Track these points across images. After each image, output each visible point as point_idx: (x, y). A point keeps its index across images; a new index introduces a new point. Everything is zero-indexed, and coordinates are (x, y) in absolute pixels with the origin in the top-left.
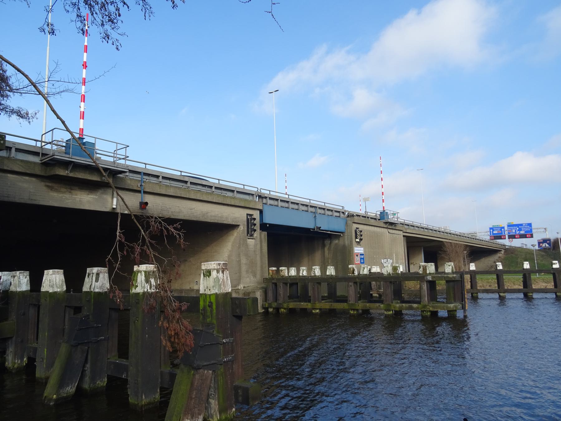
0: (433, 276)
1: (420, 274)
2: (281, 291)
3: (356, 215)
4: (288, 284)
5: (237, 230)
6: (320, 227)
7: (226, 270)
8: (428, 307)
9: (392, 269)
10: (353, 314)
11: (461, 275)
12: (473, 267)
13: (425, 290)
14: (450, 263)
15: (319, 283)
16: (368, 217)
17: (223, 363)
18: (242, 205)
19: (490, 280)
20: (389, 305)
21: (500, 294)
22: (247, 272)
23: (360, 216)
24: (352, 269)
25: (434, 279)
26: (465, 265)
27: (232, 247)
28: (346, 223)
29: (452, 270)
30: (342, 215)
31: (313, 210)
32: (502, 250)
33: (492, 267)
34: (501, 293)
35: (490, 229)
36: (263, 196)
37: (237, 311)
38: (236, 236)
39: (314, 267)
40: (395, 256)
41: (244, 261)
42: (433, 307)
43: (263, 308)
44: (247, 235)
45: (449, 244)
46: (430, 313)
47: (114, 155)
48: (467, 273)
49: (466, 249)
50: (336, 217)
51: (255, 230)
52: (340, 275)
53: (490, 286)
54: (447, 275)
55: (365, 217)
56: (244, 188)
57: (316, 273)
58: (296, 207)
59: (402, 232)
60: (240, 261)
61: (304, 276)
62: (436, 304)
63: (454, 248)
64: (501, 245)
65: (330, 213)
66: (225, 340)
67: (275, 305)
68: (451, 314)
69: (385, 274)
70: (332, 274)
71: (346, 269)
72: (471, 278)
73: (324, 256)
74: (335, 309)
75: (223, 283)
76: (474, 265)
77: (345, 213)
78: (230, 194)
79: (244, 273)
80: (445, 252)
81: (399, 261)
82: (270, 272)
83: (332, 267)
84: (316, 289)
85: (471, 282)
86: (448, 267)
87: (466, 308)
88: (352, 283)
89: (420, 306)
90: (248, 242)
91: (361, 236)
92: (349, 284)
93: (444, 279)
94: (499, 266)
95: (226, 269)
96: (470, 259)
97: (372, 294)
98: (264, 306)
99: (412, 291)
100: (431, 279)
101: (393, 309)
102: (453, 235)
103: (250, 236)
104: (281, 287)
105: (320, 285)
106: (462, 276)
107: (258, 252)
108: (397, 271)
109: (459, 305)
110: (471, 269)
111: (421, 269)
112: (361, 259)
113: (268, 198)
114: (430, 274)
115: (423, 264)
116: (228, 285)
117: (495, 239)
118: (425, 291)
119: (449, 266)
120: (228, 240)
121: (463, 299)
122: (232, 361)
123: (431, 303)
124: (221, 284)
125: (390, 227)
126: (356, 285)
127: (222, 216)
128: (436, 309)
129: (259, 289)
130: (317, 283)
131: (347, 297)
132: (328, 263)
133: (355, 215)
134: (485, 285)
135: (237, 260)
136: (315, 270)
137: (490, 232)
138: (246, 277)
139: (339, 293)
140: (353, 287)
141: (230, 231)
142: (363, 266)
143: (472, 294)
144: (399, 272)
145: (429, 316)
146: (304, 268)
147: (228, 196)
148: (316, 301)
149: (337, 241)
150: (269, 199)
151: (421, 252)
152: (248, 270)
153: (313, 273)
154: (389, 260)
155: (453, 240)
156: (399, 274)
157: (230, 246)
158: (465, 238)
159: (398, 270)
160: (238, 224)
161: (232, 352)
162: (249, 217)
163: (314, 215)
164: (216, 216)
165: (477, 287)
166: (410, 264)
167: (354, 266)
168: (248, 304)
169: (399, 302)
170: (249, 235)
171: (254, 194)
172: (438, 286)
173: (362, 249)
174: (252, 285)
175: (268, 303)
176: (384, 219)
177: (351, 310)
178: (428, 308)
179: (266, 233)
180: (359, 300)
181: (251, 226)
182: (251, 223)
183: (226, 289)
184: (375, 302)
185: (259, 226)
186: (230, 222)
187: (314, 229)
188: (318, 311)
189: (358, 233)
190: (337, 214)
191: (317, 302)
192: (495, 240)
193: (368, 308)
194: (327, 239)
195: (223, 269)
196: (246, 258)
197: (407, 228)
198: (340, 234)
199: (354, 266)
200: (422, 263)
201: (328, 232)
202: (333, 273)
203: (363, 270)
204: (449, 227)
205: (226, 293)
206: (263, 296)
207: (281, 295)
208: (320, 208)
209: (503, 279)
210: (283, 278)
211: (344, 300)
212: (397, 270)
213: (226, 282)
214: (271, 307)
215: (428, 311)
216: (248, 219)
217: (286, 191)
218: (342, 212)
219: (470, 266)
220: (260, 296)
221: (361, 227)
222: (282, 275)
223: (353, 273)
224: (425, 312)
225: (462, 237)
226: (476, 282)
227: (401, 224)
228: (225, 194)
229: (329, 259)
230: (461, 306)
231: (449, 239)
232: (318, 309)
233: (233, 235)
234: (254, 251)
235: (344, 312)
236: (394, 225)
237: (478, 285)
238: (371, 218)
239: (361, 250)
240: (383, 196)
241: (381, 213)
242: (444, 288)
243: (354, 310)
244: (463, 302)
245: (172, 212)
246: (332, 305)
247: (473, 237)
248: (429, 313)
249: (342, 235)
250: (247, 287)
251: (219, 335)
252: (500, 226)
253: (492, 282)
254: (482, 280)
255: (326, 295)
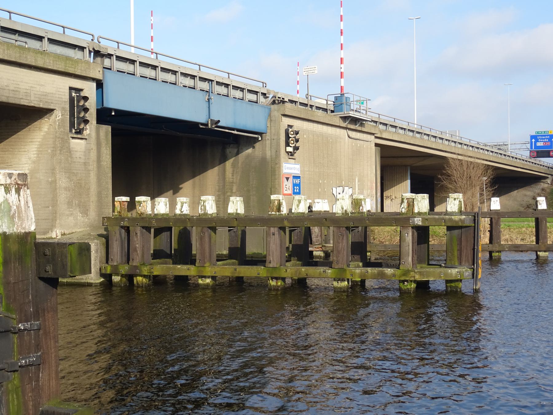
0: (424, 218)
1: (404, 214)
2: (137, 242)
3: (289, 100)
4: (152, 230)
5: (49, 119)
6: (219, 121)
7: (26, 188)
8: (412, 273)
9: (352, 203)
10: (276, 286)
11: (475, 217)
12: (496, 204)
13: (409, 244)
14: (455, 195)
15: (214, 229)
16: (311, 106)
17: (17, 368)
18: (61, 68)
19: (524, 229)
20: (343, 270)
21: (538, 253)
22: (70, 204)
23: (296, 102)
24: (276, 202)
25: (427, 224)
26: (482, 202)
27: (38, 154)
28: (270, 115)
29: (460, 208)
30: (262, 99)
31: (205, 86)
32: (549, 176)
33: (529, 208)
34: (540, 251)
35: (532, 137)
36: (103, 51)
37: (48, 268)
38: (46, 132)
39: (203, 198)
40: (358, 182)
41: (63, 182)
42: (421, 273)
43: (102, 275)
44: (71, 131)
45: (457, 162)
46: (415, 285)
48: (485, 215)
49: (487, 172)
50: (250, 102)
51: (86, 122)
52: (255, 213)
53: (522, 239)
54: (450, 217)
55: (306, 105)
56: (64, 32)
57: (207, 208)
58: (170, 78)
59: (373, 137)
60: (55, 182)
61: (185, 215)
62: (427, 268)
63: (465, 169)
64: (547, 168)
65: (238, 94)
66: (24, 325)
67: (124, 269)
68: (451, 287)
69: (338, 214)
70: (239, 212)
71: (265, 201)
72: (491, 225)
73: (224, 178)
74: (242, 277)
75: (19, 213)
76: (499, 201)
77: (267, 95)
78: (33, 44)
79: (62, 207)
80: (450, 176)
81: (365, 192)
82: (117, 204)
83: (238, 198)
84: (207, 239)
85: (491, 231)
86: (453, 201)
87: (479, 276)
88: (276, 229)
89: (398, 272)
90: (72, 146)
91: (297, 141)
92: (270, 230)
93: (443, 224)
94: (540, 204)
95: (25, 185)
96: (493, 190)
97: (312, 252)
98: (103, 272)
99: (385, 246)
100: (420, 223)
101: (350, 277)
102: (465, 147)
103: (76, 133)
104: (139, 234)
105: (215, 233)
106: (476, 218)
107: (93, 166)
108: (361, 208)
109: (466, 271)
110: (493, 208)
111: (405, 205)
112: (294, 185)
113: (114, 57)
114: (419, 214)
115: (409, 195)
116: (30, 218)
117: (538, 157)
118: (409, 246)
119: (455, 199)
120: (30, 140)
121: (474, 261)
122: (37, 365)
123: (418, 268)
124: (14, 214)
125: (352, 127)
126: (283, 233)
127: (16, 89)
128: (427, 278)
129: (94, 239)
130: (209, 228)
131: (265, 257)
132: (232, 192)
133: (286, 100)
134: (515, 238)
135: (48, 181)
136: (206, 204)
137: (531, 142)
138: (67, 215)
139: (251, 249)
140: (277, 236)
141: (35, 121)
142: (297, 197)
143: (491, 253)
144: (365, 210)
145: (412, 290)
146: (184, 199)
147: (29, 49)
148: (205, 263)
149: (250, 151)
150: (116, 59)
151: (406, 176)
152: (72, 201)
153: (201, 209)
154: (346, 188)
155: (465, 156)
156: (363, 213)
157: (35, 152)
158: (486, 152)
159: (363, 207)
160: (52, 107)
161: (38, 347)
162: (74, 94)
163: (207, 97)
164: (4, 89)
165: (500, 241)
166: (384, 198)
167: (280, 197)
168: (71, 255)
169: (361, 264)
170: (74, 131)
171: (86, 48)
172: (432, 237)
173: (298, 166)
174: (78, 230)
175: (112, 266)
176: (342, 111)
177: (272, 278)
178: (412, 275)
179: (109, 128)
180: (287, 261)
181: (79, 113)
182: (78, 106)
183: (24, 226)
184: (316, 264)
185: (95, 113)
186: (33, 101)
187: (206, 125)
188: (208, 281)
189: (290, 136)
190: (253, 97)
191: (207, 264)
192: (538, 159)
193: (303, 275)
194: (232, 145)
195: (18, 184)
196: (68, 178)
197: (383, 131)
198: (256, 136)
199: (280, 197)
200: (406, 193)
201: (233, 132)
202: (241, 210)
203: (298, 206)
204: (459, 131)
205: (26, 233)
206: (101, 253)
207: (137, 251)
208: (218, 83)
209: (546, 227)
210: (143, 218)
211: (259, 260)
212: (361, 205)
213: (25, 211)
214: (117, 274)
215: (411, 281)
216: (72, 99)
217: (152, 45)
218: (262, 93)
219: (492, 203)
220: (95, 252)
221: (297, 124)
222: (139, 212)
223: (279, 210)
224: (406, 283)
225: (481, 151)
226: (500, 232)
227: (373, 121)
228: (24, 44)
229: (234, 184)
230: (470, 271)
231: (458, 154)
232: (209, 277)
233: (40, 129)
234: (85, 164)
235: (262, 284)
236: (360, 123)
237: (503, 238)
238: (316, 107)
239: (294, 168)
240: (342, 66)
241: (336, 98)
242: (443, 243)
243: (277, 278)
244: (474, 265)
246: (235, 270)
247: (500, 148)
248: (413, 285)
249: (260, 139)
250: (69, 234)
251: (10, 315)
252: (550, 133)
253: (528, 232)
254: (510, 229)
255: (225, 252)
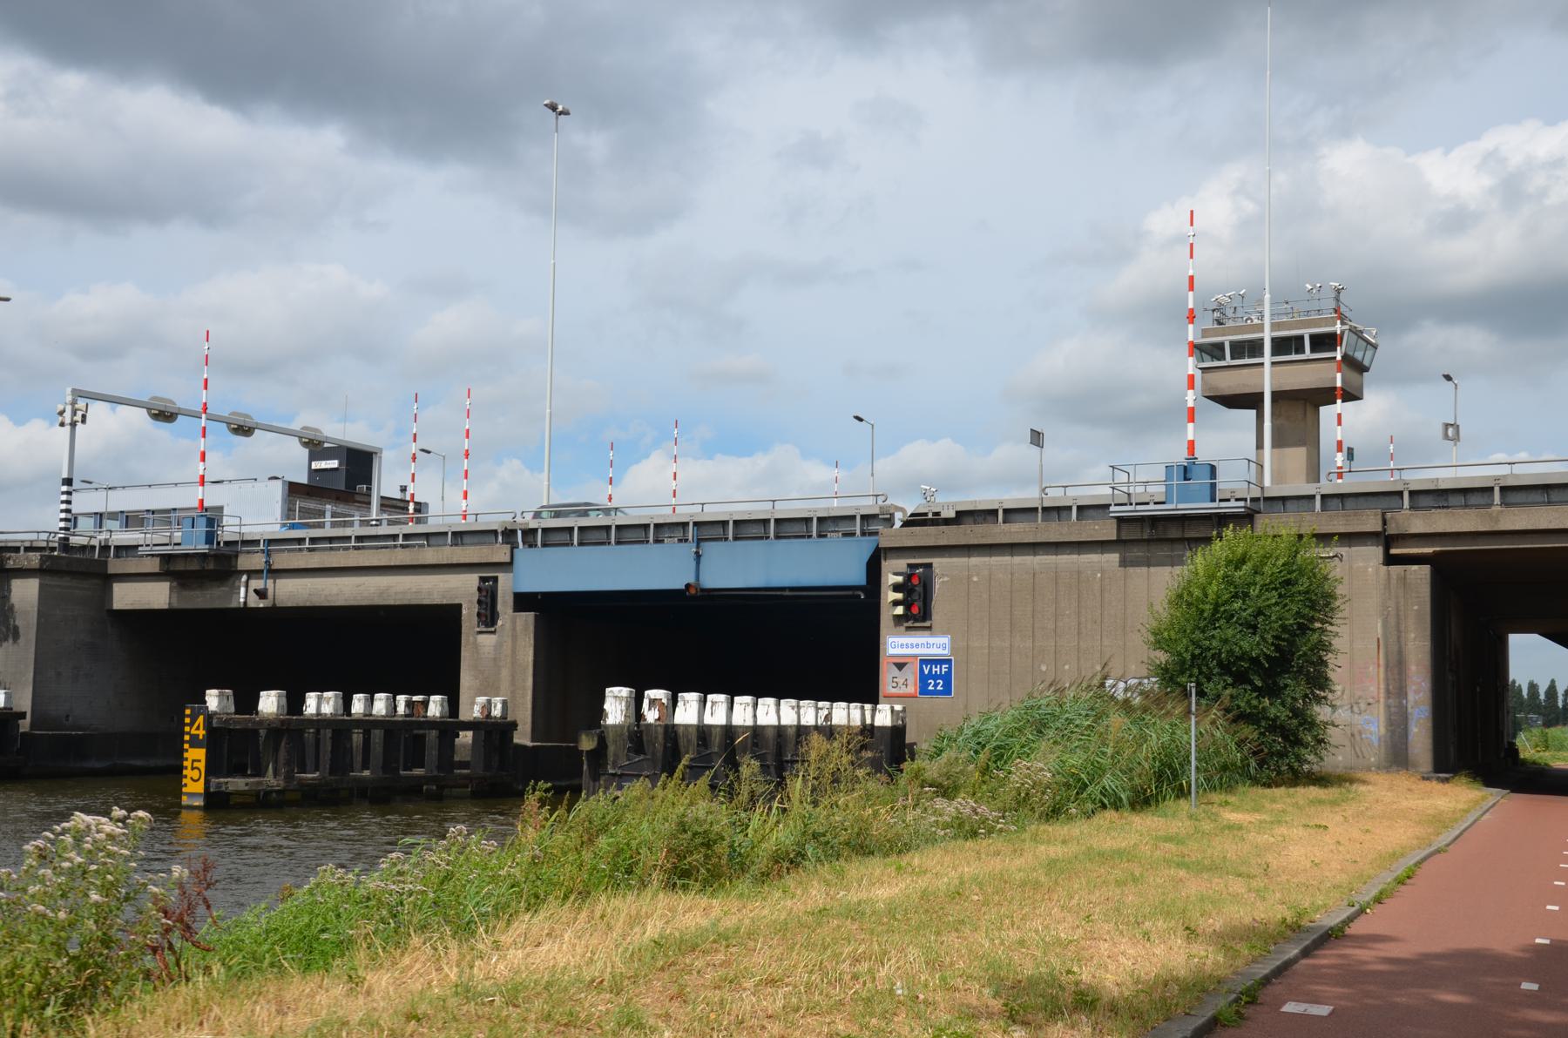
47: (1129, 489)
234: (495, 659)
245: (326, 596)
